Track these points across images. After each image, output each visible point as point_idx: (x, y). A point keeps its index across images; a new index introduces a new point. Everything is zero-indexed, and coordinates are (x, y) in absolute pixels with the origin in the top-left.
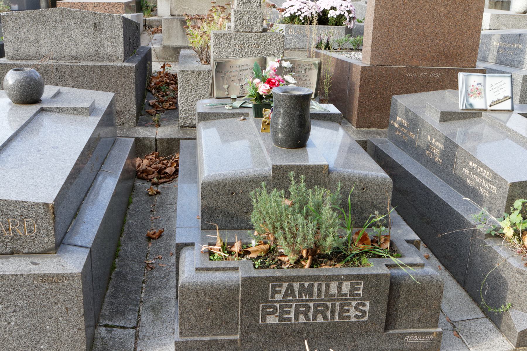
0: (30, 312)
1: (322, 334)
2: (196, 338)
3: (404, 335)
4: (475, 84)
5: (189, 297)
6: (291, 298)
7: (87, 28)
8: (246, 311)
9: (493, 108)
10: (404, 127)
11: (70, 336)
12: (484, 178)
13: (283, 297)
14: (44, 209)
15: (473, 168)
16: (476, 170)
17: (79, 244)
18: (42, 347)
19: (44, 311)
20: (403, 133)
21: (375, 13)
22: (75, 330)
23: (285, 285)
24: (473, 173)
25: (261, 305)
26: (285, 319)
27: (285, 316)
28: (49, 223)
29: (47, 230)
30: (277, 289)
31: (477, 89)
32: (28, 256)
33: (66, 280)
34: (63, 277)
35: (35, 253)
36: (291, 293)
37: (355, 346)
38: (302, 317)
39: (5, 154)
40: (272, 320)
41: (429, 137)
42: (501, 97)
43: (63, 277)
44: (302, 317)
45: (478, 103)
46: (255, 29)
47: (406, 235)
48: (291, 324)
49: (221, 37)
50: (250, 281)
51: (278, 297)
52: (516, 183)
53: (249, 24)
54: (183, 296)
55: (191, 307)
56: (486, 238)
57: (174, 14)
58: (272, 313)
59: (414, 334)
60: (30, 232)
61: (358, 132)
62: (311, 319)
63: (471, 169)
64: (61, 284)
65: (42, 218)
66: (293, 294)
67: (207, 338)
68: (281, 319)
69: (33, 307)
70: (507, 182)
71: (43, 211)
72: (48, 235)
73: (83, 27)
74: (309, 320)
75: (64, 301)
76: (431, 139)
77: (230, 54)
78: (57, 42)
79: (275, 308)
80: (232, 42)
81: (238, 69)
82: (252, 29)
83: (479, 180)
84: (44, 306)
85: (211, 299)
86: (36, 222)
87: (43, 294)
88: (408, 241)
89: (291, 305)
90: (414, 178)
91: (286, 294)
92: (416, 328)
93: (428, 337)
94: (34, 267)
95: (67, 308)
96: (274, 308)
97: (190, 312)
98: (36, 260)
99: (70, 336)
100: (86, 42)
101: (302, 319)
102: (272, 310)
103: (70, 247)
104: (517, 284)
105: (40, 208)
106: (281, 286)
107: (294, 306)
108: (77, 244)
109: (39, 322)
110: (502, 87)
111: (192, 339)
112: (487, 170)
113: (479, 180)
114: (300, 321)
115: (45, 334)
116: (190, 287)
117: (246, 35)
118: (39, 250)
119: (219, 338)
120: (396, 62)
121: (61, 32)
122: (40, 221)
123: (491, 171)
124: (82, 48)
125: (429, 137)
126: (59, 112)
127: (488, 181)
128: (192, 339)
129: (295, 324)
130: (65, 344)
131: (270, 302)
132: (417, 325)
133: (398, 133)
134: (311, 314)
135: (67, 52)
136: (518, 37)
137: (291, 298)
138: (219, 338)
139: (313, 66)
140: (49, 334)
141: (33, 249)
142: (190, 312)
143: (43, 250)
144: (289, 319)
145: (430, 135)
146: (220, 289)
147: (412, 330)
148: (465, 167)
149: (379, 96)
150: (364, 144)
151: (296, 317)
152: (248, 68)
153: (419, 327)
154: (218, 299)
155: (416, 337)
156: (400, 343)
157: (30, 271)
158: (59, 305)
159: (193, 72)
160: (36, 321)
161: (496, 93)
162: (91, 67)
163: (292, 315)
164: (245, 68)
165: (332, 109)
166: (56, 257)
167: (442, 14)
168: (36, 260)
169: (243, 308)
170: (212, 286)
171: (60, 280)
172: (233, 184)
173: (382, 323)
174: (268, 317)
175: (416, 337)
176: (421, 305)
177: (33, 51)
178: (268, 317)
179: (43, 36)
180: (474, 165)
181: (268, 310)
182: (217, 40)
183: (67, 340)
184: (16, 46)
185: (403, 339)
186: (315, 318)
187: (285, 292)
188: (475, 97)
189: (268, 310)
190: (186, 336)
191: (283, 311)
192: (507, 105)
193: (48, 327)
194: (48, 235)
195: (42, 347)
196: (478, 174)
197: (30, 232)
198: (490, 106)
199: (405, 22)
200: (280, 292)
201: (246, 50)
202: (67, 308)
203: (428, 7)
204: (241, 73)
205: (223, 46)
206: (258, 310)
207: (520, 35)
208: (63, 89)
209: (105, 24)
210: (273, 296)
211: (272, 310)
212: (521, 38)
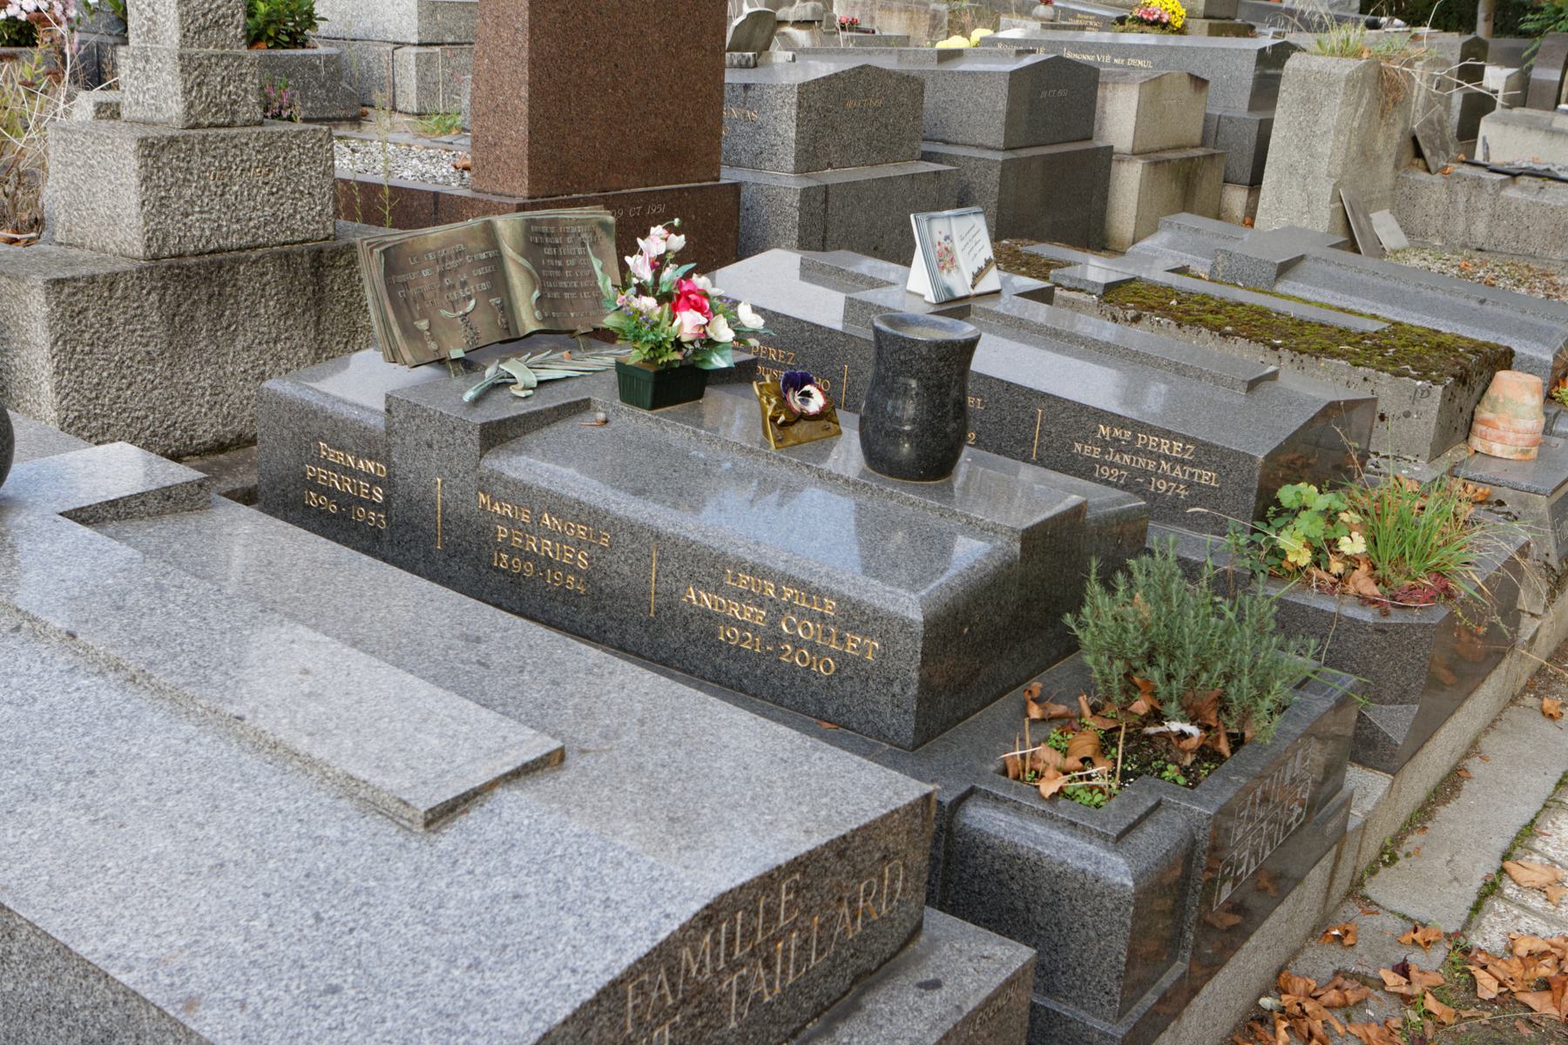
46: (244, 113)
49: (163, 148)
53: (224, 98)
63: (1104, 445)
70: (1252, 458)
77: (192, 204)
80: (196, 164)
82: (234, 113)
117: (232, 138)
120: (579, 184)
123: (1187, 439)
126: (118, 517)
136: (740, 91)
159: (92, 279)
167: (656, 47)
180: (1117, 433)
182: (150, 162)
198: (973, 286)
199: (590, 72)
201: (236, 188)
205: (170, 180)
207: (746, 87)
212: (750, 93)
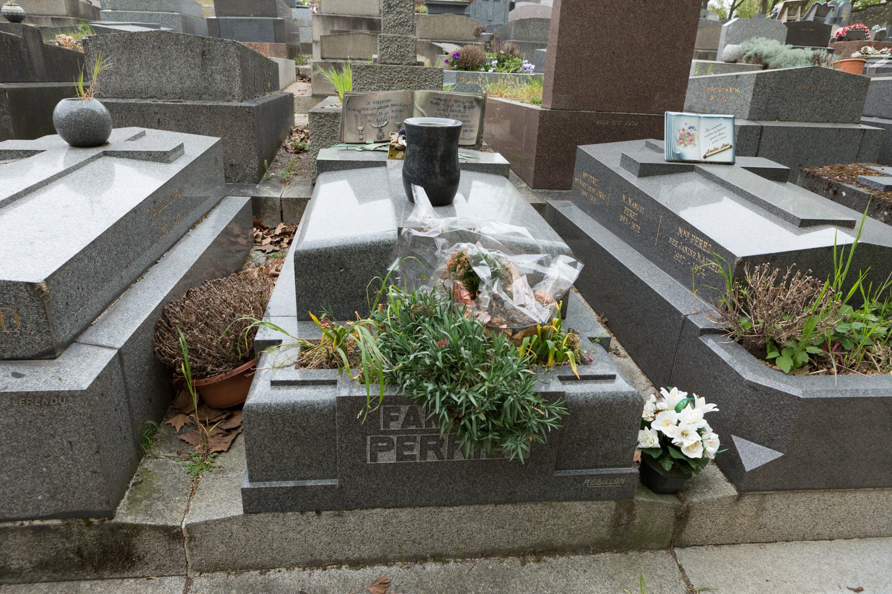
0: (14, 448)
1: (462, 477)
2: (275, 484)
3: (582, 478)
4: (686, 128)
5: (260, 425)
6: (414, 428)
7: (193, 58)
8: (347, 446)
9: (708, 159)
10: (592, 185)
11: (81, 482)
12: (700, 250)
13: (403, 426)
14: (27, 291)
15: (684, 237)
16: (689, 240)
17: (104, 343)
18: (40, 497)
19: (35, 447)
20: (590, 193)
21: (558, 42)
22: (88, 473)
23: (404, 409)
24: (684, 244)
25: (369, 438)
26: (407, 457)
27: (406, 453)
28: (38, 312)
29: (38, 324)
30: (393, 414)
31: (689, 134)
32: (11, 364)
33: (62, 401)
34: (58, 396)
35: (24, 359)
36: (414, 420)
37: (511, 493)
38: (430, 453)
39: (4, 210)
40: (387, 458)
41: (624, 197)
42: (719, 145)
43: (58, 396)
44: (430, 453)
45: (691, 153)
47: (591, 330)
48: (416, 464)
50: (350, 402)
51: (394, 426)
52: (747, 257)
54: (249, 423)
55: (263, 439)
56: (701, 335)
57: (325, 56)
58: (388, 449)
59: (598, 476)
60: (10, 327)
61: (534, 193)
62: (446, 457)
63: (680, 239)
64: (57, 408)
65: (27, 306)
66: (417, 422)
67: (291, 484)
68: (400, 456)
69: (17, 441)
71: (26, 295)
72: (39, 331)
73: (188, 56)
74: (442, 457)
75: (65, 432)
76: (627, 200)
78: (156, 75)
79: (390, 441)
81: (376, 106)
83: (692, 253)
84: (34, 439)
85: (294, 427)
86: (17, 312)
87: (30, 422)
88: (592, 339)
89: (415, 437)
90: (603, 249)
91: (407, 422)
92: (601, 467)
93: (617, 482)
94: (14, 380)
95: (70, 443)
96: (389, 442)
97: (263, 447)
98: (20, 370)
99: (81, 482)
100: (192, 76)
101: (431, 457)
102: (385, 444)
103: (85, 347)
104: (747, 404)
105: (21, 291)
106: (398, 410)
107: (419, 439)
108: (100, 343)
109: (30, 462)
110: (721, 132)
111: (268, 484)
112: (704, 240)
113: (692, 253)
114: (429, 460)
115: (42, 479)
116: (260, 411)
118: (29, 354)
119: (310, 483)
120: (584, 106)
121: (160, 62)
122: (23, 309)
124: (188, 83)
125: (624, 197)
127: (706, 254)
128: (268, 484)
129: (421, 464)
130: (74, 493)
131: (382, 433)
132: (603, 464)
133: (584, 193)
134: (444, 450)
135: (169, 88)
137: (414, 428)
138: (310, 483)
139: (474, 104)
140: (47, 480)
141: (19, 353)
142: (263, 447)
143: (34, 354)
144: (413, 457)
145: (626, 194)
146: (306, 414)
147: (594, 471)
148: (673, 235)
149: (562, 148)
150: (540, 208)
151: (423, 454)
152: (389, 104)
153: (605, 466)
154: (304, 429)
155: (599, 481)
156: (577, 489)
157: (6, 388)
158: (58, 438)
160: (24, 461)
161: (714, 140)
162: (199, 107)
163: (416, 452)
164: (385, 104)
165: (498, 159)
166: (51, 366)
168: (20, 370)
169: (343, 442)
170: (294, 411)
171: (54, 401)
172: (341, 256)
173: (551, 461)
174: (380, 454)
175: (599, 481)
176: (608, 436)
177: (127, 84)
178: (380, 454)
179: (137, 66)
181: (380, 444)
183: (77, 488)
184: (103, 80)
185: (580, 483)
186: (451, 455)
187: (405, 419)
188: (686, 145)
189: (380, 444)
190: (259, 480)
191: (404, 446)
192: (727, 156)
193: (44, 469)
194: (40, 332)
195: (40, 497)
196: (690, 246)
197: (10, 327)
200: (397, 418)
202: (70, 443)
203: (626, 36)
204: (380, 110)
206: (365, 445)
208: (147, 130)
209: (216, 52)
210: (386, 425)
211: (385, 444)
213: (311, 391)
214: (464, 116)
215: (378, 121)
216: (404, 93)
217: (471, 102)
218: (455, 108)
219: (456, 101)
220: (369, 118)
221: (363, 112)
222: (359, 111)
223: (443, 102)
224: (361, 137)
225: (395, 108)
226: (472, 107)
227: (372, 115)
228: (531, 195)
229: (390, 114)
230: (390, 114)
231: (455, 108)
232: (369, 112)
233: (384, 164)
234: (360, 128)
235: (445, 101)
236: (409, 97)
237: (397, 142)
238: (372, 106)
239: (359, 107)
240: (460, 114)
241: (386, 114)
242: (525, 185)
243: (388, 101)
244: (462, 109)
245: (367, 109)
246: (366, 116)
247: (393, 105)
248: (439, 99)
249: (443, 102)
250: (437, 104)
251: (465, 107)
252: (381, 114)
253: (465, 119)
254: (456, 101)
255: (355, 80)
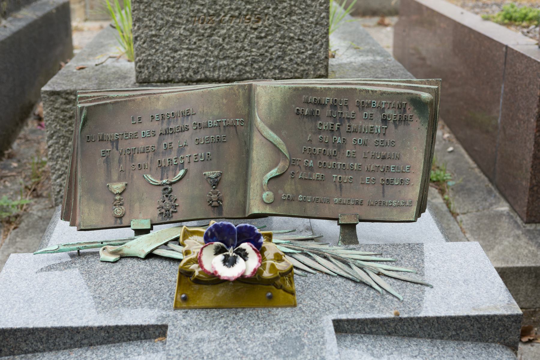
61: (532, 236)
81: (158, 127)
139: (410, 111)
152: (188, 122)
204: (168, 139)
213: (254, 152)
214: (383, 144)
215: (163, 169)
216: (226, 94)
217: (402, 108)
218: (359, 123)
219: (362, 106)
220: (140, 158)
221: (124, 145)
222: (115, 142)
223: (328, 110)
224: (118, 211)
225: (203, 134)
226: (403, 120)
227: (145, 151)
228: (523, 241)
229: (192, 150)
230: (192, 150)
231: (359, 123)
232: (141, 144)
233: (154, 333)
234: (117, 187)
235: (334, 106)
236: (241, 102)
237: (198, 261)
238: (147, 126)
239: (112, 133)
240: (373, 139)
241: (181, 149)
242: (504, 208)
243: (187, 115)
244: (378, 126)
245: (135, 136)
246: (131, 153)
247: (199, 126)
248: (319, 104)
249: (328, 110)
250: (313, 116)
251: (385, 121)
252: (168, 149)
253: (387, 151)
254: (362, 106)
255: (138, 20)
